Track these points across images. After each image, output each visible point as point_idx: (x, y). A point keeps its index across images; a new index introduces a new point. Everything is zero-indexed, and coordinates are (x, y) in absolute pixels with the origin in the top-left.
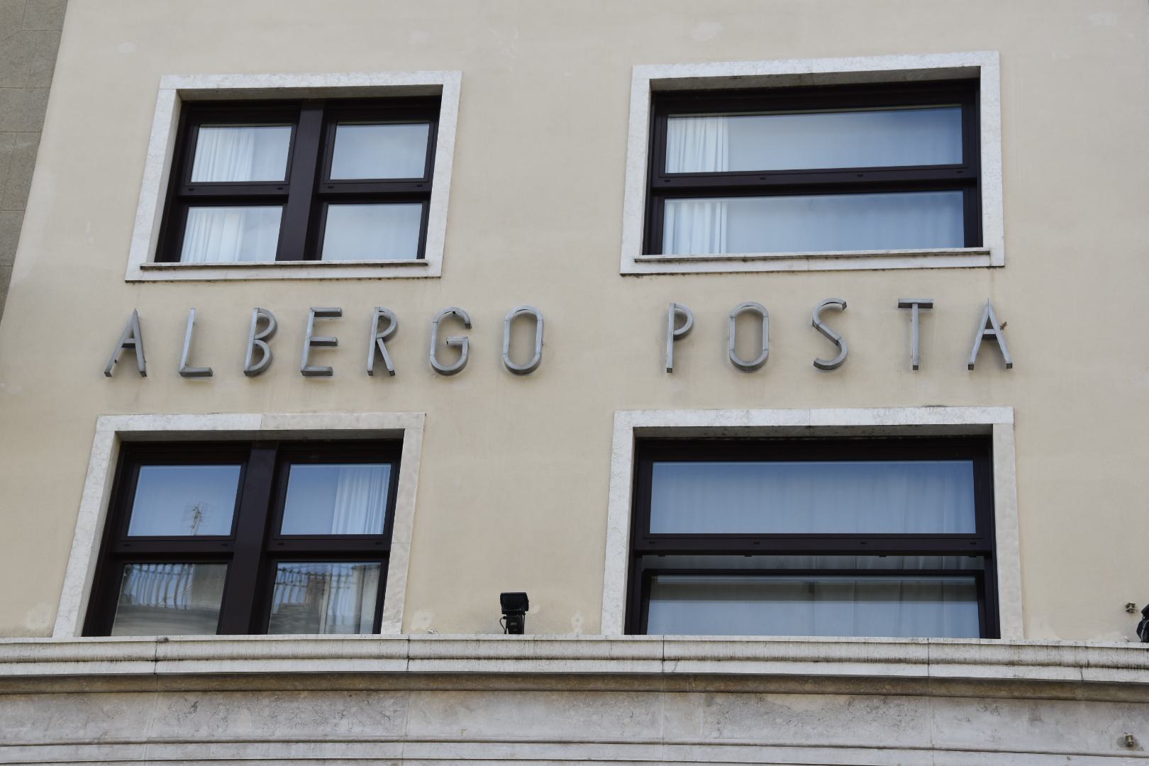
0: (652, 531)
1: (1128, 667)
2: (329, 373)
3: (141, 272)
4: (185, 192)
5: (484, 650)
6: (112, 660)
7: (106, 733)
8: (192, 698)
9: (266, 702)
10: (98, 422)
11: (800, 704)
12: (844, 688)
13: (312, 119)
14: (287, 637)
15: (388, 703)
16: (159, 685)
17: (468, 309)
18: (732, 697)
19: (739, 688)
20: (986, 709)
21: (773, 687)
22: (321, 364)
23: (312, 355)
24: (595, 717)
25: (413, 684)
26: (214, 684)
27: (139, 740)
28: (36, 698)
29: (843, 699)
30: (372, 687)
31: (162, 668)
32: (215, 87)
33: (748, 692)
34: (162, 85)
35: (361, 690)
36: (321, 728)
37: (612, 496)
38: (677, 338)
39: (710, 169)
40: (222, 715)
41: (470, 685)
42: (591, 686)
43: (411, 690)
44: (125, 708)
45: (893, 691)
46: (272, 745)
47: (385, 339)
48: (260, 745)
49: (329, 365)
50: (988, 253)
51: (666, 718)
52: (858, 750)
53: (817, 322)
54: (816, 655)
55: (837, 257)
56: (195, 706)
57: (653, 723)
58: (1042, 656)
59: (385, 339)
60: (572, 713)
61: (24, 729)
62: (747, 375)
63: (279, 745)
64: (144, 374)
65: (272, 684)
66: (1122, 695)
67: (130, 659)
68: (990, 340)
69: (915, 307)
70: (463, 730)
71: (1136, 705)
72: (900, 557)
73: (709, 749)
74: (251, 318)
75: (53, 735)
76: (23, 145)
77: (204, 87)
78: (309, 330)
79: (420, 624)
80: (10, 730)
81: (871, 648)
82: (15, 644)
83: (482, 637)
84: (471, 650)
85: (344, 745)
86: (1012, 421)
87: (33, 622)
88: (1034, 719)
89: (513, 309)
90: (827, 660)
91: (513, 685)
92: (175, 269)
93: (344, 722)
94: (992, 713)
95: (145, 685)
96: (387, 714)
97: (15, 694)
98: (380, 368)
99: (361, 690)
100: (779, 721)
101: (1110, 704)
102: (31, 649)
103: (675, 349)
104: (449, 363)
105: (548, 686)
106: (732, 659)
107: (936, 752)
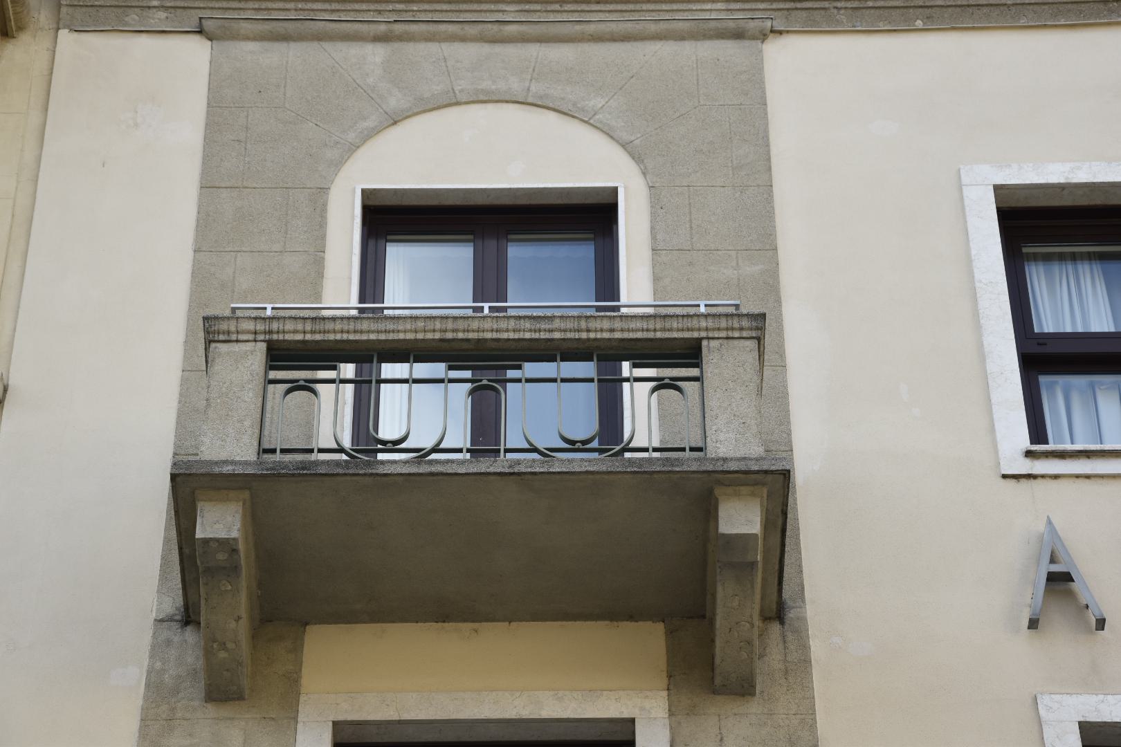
34: (965, 180)
68: (1059, 581)
72: (551, 470)
76: (752, 269)
92: (1047, 457)
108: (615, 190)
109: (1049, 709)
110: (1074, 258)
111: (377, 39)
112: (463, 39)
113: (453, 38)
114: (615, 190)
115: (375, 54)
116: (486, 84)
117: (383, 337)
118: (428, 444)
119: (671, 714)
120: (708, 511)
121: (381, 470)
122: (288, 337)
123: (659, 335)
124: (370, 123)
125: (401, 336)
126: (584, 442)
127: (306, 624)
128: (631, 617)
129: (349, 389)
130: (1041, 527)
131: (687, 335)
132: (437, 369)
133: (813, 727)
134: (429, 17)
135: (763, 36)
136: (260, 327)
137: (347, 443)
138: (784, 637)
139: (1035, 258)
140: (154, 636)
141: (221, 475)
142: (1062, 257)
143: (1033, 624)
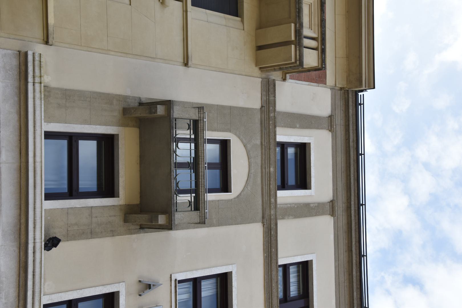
0: (79, 141)
3: (174, 280)
6: (34, 272)
10: (123, 283)
14: (43, 115)
28: (17, 299)
32: (233, 285)
34: (233, 265)
39: (202, 295)
77: (233, 281)
82: (41, 289)
87: (47, 287)
97: (19, 290)
102: (38, 296)
109: (122, 285)
110: (217, 288)
112: (262, 160)
113: (262, 158)
115: (258, 142)
117: (200, 144)
118: (177, 153)
119: (120, 205)
120: (163, 213)
122: (200, 124)
123: (201, 202)
125: (200, 148)
127: (139, 128)
128: (141, 197)
129: (189, 137)
130: (161, 283)
131: (201, 208)
132: (193, 155)
135: (263, 223)
138: (137, 229)
142: (217, 286)
143: (140, 281)
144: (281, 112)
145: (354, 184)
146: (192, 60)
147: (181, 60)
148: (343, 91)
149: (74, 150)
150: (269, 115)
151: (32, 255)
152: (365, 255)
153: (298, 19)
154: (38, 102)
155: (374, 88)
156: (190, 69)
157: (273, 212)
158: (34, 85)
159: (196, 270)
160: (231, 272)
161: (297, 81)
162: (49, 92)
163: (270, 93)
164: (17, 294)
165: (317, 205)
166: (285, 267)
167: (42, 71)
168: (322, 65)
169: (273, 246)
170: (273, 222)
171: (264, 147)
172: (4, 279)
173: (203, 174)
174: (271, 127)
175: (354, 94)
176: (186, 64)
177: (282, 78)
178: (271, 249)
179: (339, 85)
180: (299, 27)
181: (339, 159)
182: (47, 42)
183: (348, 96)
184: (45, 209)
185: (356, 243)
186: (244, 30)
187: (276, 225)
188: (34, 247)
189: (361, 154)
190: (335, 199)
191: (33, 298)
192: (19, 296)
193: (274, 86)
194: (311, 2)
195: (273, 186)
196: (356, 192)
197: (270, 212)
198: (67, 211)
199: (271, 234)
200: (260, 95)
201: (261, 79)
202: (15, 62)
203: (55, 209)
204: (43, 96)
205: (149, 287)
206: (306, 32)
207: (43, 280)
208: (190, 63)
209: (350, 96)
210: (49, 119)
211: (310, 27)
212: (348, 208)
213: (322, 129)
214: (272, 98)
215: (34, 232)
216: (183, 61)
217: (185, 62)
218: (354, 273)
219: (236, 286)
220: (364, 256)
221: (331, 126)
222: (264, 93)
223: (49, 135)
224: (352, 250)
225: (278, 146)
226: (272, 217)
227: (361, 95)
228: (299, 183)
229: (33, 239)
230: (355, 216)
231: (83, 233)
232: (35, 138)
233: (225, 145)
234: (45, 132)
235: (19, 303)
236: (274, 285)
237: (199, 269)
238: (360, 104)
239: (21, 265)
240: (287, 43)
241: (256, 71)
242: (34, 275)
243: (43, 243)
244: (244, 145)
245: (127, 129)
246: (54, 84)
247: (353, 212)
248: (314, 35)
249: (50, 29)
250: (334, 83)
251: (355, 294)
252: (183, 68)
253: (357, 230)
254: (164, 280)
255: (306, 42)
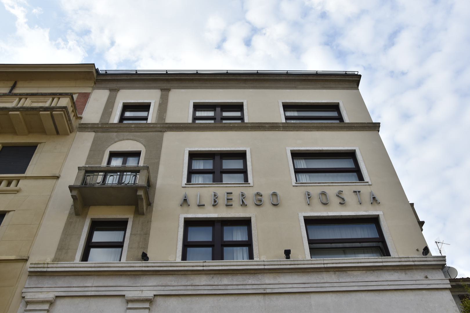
1: (423, 261)
2: (232, 205)
4: (91, 244)
5: (282, 263)
7: (192, 284)
8: (212, 276)
9: (230, 276)
11: (356, 273)
12: (364, 269)
13: (217, 158)
15: (260, 276)
16: (204, 273)
17: (262, 193)
18: (340, 272)
19: (341, 270)
20: (395, 272)
21: (348, 269)
22: (230, 203)
23: (227, 202)
24: (309, 278)
25: (265, 271)
26: (217, 272)
27: (201, 285)
28: (174, 276)
29: (364, 272)
30: (255, 272)
31: (205, 268)
33: (343, 271)
34: (185, 150)
35: (253, 273)
36: (244, 282)
37: (302, 230)
38: (309, 198)
40: (220, 279)
41: (279, 271)
42: (307, 271)
43: (265, 273)
44: (196, 278)
45: (375, 269)
46: (234, 286)
47: (244, 198)
48: (231, 286)
49: (232, 203)
50: (249, 184)
51: (326, 277)
52: (371, 282)
53: (338, 194)
54: (358, 261)
55: (338, 183)
56: (213, 277)
57: (323, 278)
58: (406, 259)
59: (244, 198)
60: (304, 277)
61: (172, 283)
62: (324, 205)
63: (236, 286)
64: (189, 205)
65: (231, 272)
66: (422, 267)
67: (197, 266)
68: (185, 200)
69: (357, 192)
70: (279, 282)
71: (425, 270)
73: (338, 283)
74: (212, 194)
75: (179, 284)
78: (226, 196)
79: (263, 258)
80: (169, 283)
81: (370, 259)
83: (281, 260)
84: (279, 263)
85: (251, 286)
86: (383, 214)
87: (171, 259)
88: (406, 274)
89: (271, 192)
90: (361, 263)
91: (289, 271)
93: (250, 280)
94: (397, 273)
95: (200, 273)
96: (260, 278)
98: (243, 204)
99: (253, 273)
100: (351, 277)
101: (420, 270)
103: (309, 200)
104: (258, 203)
105: (297, 271)
106: (339, 263)
107: (388, 282)
108: (355, 150)
109: (181, 216)
110: (200, 160)
111: (116, 132)
112: (127, 132)
113: (125, 132)
114: (355, 150)
115: (115, 134)
116: (128, 138)
117: (100, 169)
118: (127, 183)
119: (134, 217)
120: (136, 191)
121: (94, 186)
122: (88, 170)
123: (135, 169)
124: (112, 143)
125: (102, 169)
126: (99, 183)
127: (90, 206)
128: (131, 205)
129: (118, 176)
130: (184, 193)
131: (138, 169)
132: (130, 173)
133: (151, 219)
134: (123, 129)
135: (164, 132)
136: (85, 168)
137: (117, 183)
138: (150, 208)
139: (194, 160)
140: (71, 207)
141: (75, 187)
142: (199, 160)
143: (372, 203)
144: (100, 120)
145: (153, 77)
146: (56, 174)
147: (54, 181)
148: (97, 83)
149: (97, 244)
150: (100, 128)
151: (149, 268)
152: (257, 71)
153: (37, 110)
154: (59, 265)
155: (94, 64)
156: (62, 175)
157: (159, 126)
158: (49, 268)
159: (183, 172)
160: (291, 150)
161: (84, 110)
162: (56, 259)
163: (86, 127)
164: (219, 275)
165: (161, 99)
166: (287, 118)
167: (41, 263)
168: (69, 95)
169: (179, 126)
170: (165, 126)
171: (118, 131)
172: (161, 283)
173: (118, 168)
174: (107, 126)
175: (99, 76)
176: (58, 177)
177: (80, 119)
178: (180, 127)
179: (93, 85)
180: (42, 109)
181: (137, 85)
182: (26, 260)
183: (99, 79)
184: (126, 261)
185: (188, 76)
186: (45, 142)
187: (167, 124)
188: (145, 267)
189: (197, 72)
190: (160, 88)
191: (174, 266)
192: (172, 274)
193: (83, 124)
194: (30, 101)
195: (342, 125)
196: (158, 75)
197: (159, 127)
198: (130, 248)
199: (172, 127)
200: (87, 133)
201: (78, 132)
202: (34, 279)
203: (127, 255)
204: (56, 263)
205: (185, 200)
206: (47, 105)
207: (167, 262)
208: (57, 175)
209: (99, 78)
210: (73, 259)
211: (46, 102)
212: (167, 80)
213: (116, 96)
214: (90, 126)
215: (136, 267)
216: (56, 180)
217: (57, 178)
218: (206, 78)
219: (198, 148)
220: (227, 72)
221: (116, 90)
222: (86, 130)
223: (184, 257)
224: (192, 79)
225: (123, 122)
226: (162, 126)
227: (101, 72)
228: (213, 109)
229: (140, 268)
230: (172, 76)
231: (145, 239)
232: (80, 267)
233: (113, 155)
234: (182, 260)
235: (176, 274)
236: (202, 126)
237: (183, 170)
238: (106, 72)
239: (155, 274)
240: (52, 116)
241: (72, 135)
242: (161, 267)
243: (143, 262)
244: (114, 143)
245: (89, 213)
246: (53, 256)
247: (169, 78)
248: (51, 99)
249: (18, 258)
250: (90, 88)
251: (218, 78)
252: (60, 180)
253: (180, 75)
254: (183, 192)
255: (53, 105)
